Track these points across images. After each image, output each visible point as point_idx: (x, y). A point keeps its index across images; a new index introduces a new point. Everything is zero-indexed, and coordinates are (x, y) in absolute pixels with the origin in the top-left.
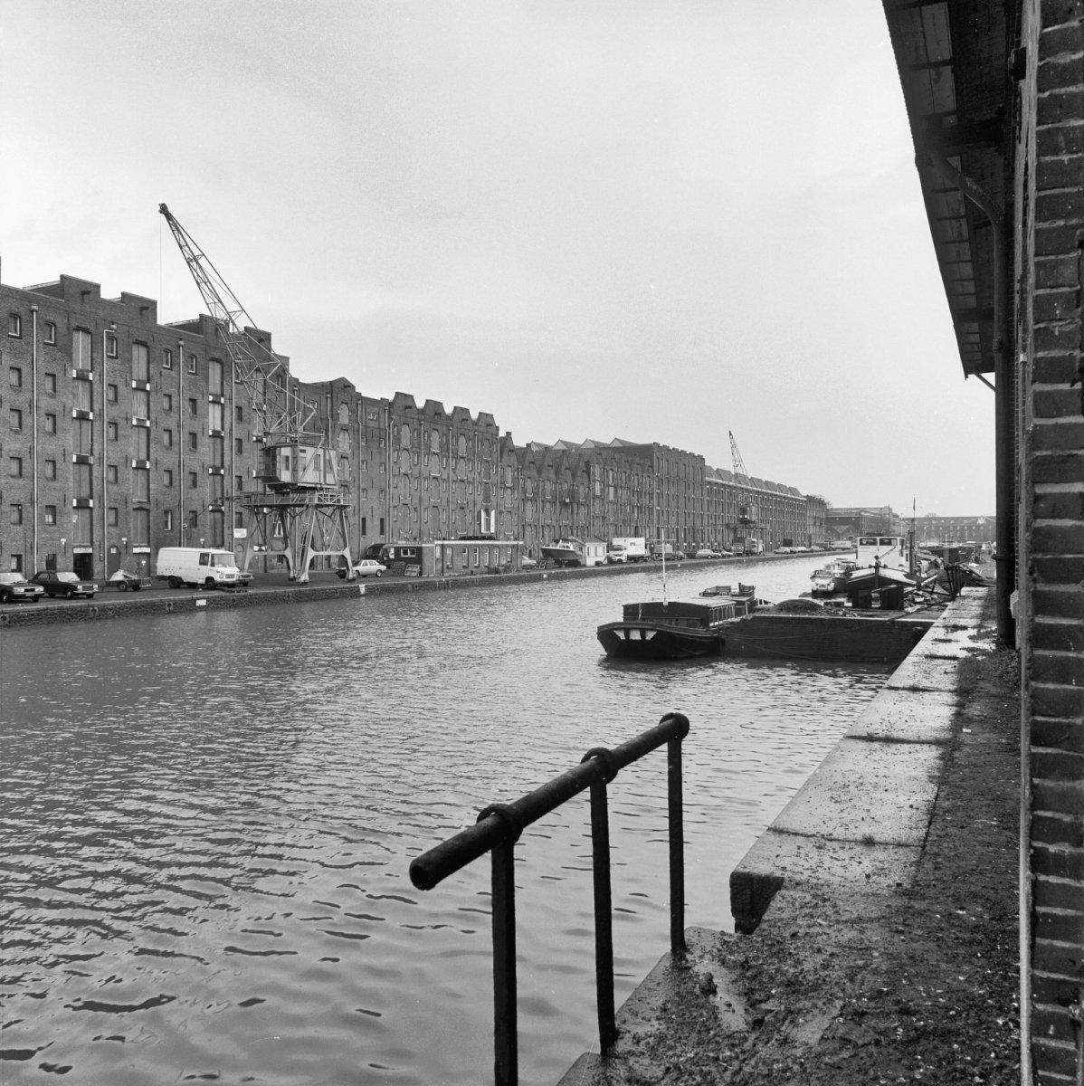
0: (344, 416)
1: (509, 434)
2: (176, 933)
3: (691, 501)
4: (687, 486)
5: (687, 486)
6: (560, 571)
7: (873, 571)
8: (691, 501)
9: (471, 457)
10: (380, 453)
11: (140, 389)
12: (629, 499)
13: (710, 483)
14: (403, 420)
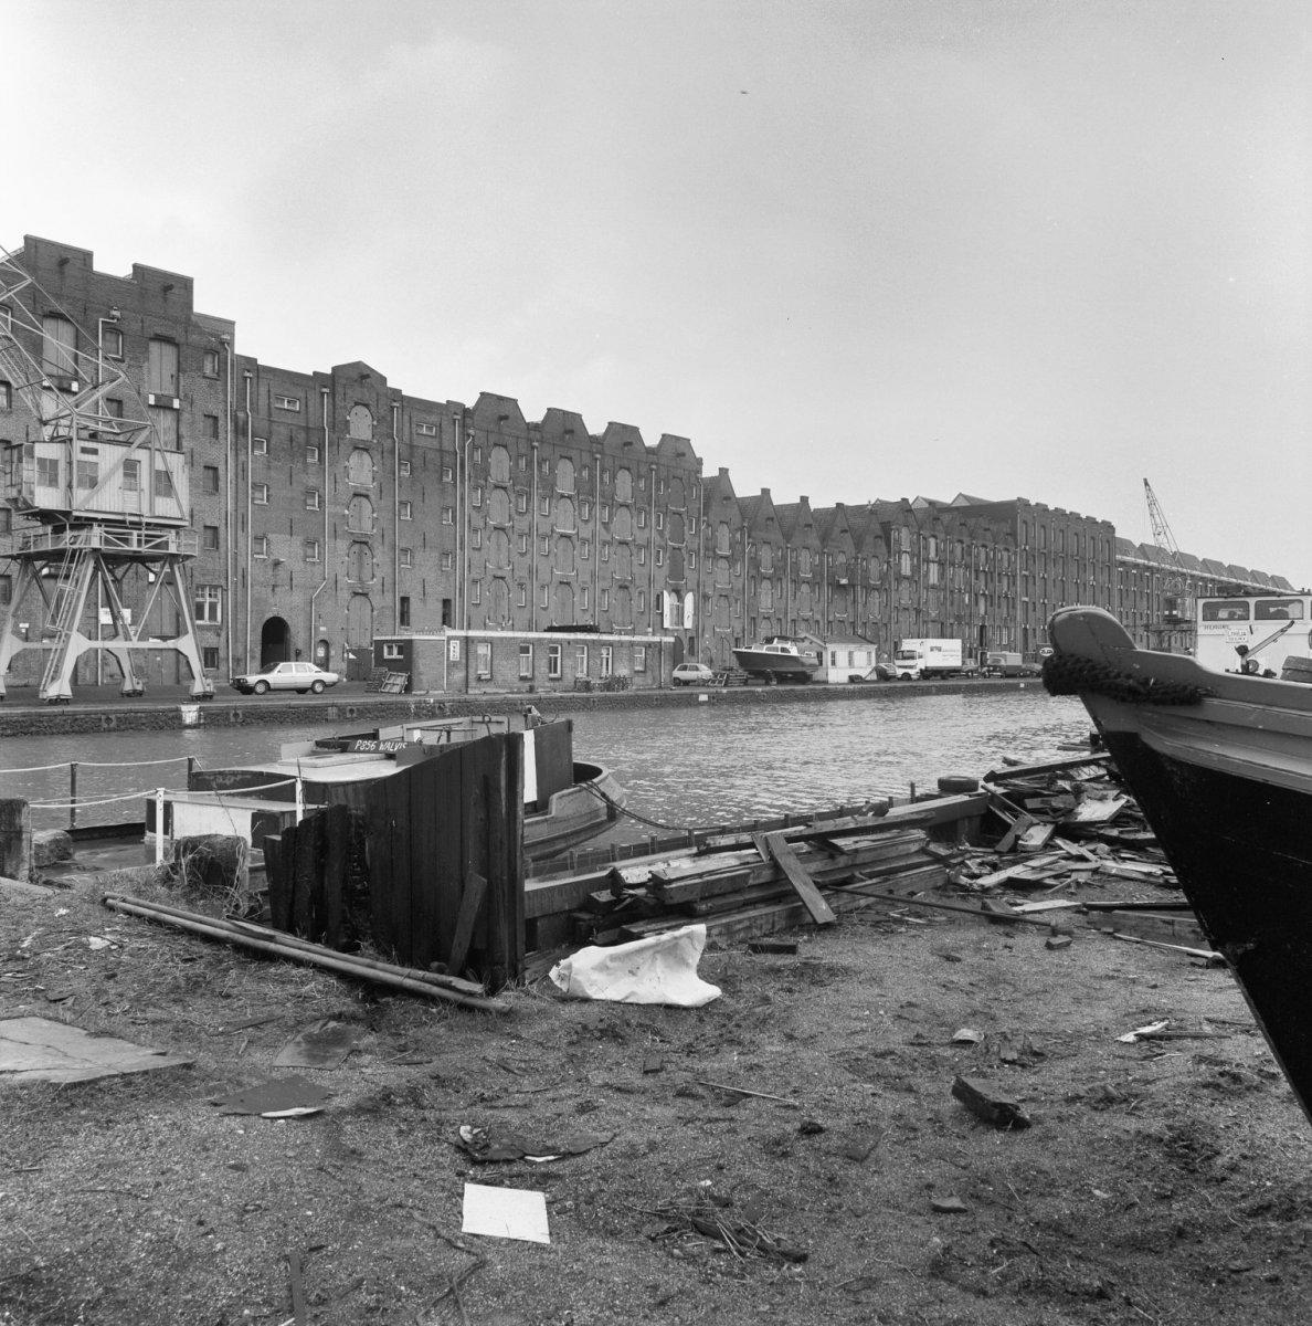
0: (361, 425)
1: (723, 471)
3: (1131, 596)
6: (768, 688)
8: (1131, 596)
10: (443, 491)
11: (162, 405)
13: (1123, 563)
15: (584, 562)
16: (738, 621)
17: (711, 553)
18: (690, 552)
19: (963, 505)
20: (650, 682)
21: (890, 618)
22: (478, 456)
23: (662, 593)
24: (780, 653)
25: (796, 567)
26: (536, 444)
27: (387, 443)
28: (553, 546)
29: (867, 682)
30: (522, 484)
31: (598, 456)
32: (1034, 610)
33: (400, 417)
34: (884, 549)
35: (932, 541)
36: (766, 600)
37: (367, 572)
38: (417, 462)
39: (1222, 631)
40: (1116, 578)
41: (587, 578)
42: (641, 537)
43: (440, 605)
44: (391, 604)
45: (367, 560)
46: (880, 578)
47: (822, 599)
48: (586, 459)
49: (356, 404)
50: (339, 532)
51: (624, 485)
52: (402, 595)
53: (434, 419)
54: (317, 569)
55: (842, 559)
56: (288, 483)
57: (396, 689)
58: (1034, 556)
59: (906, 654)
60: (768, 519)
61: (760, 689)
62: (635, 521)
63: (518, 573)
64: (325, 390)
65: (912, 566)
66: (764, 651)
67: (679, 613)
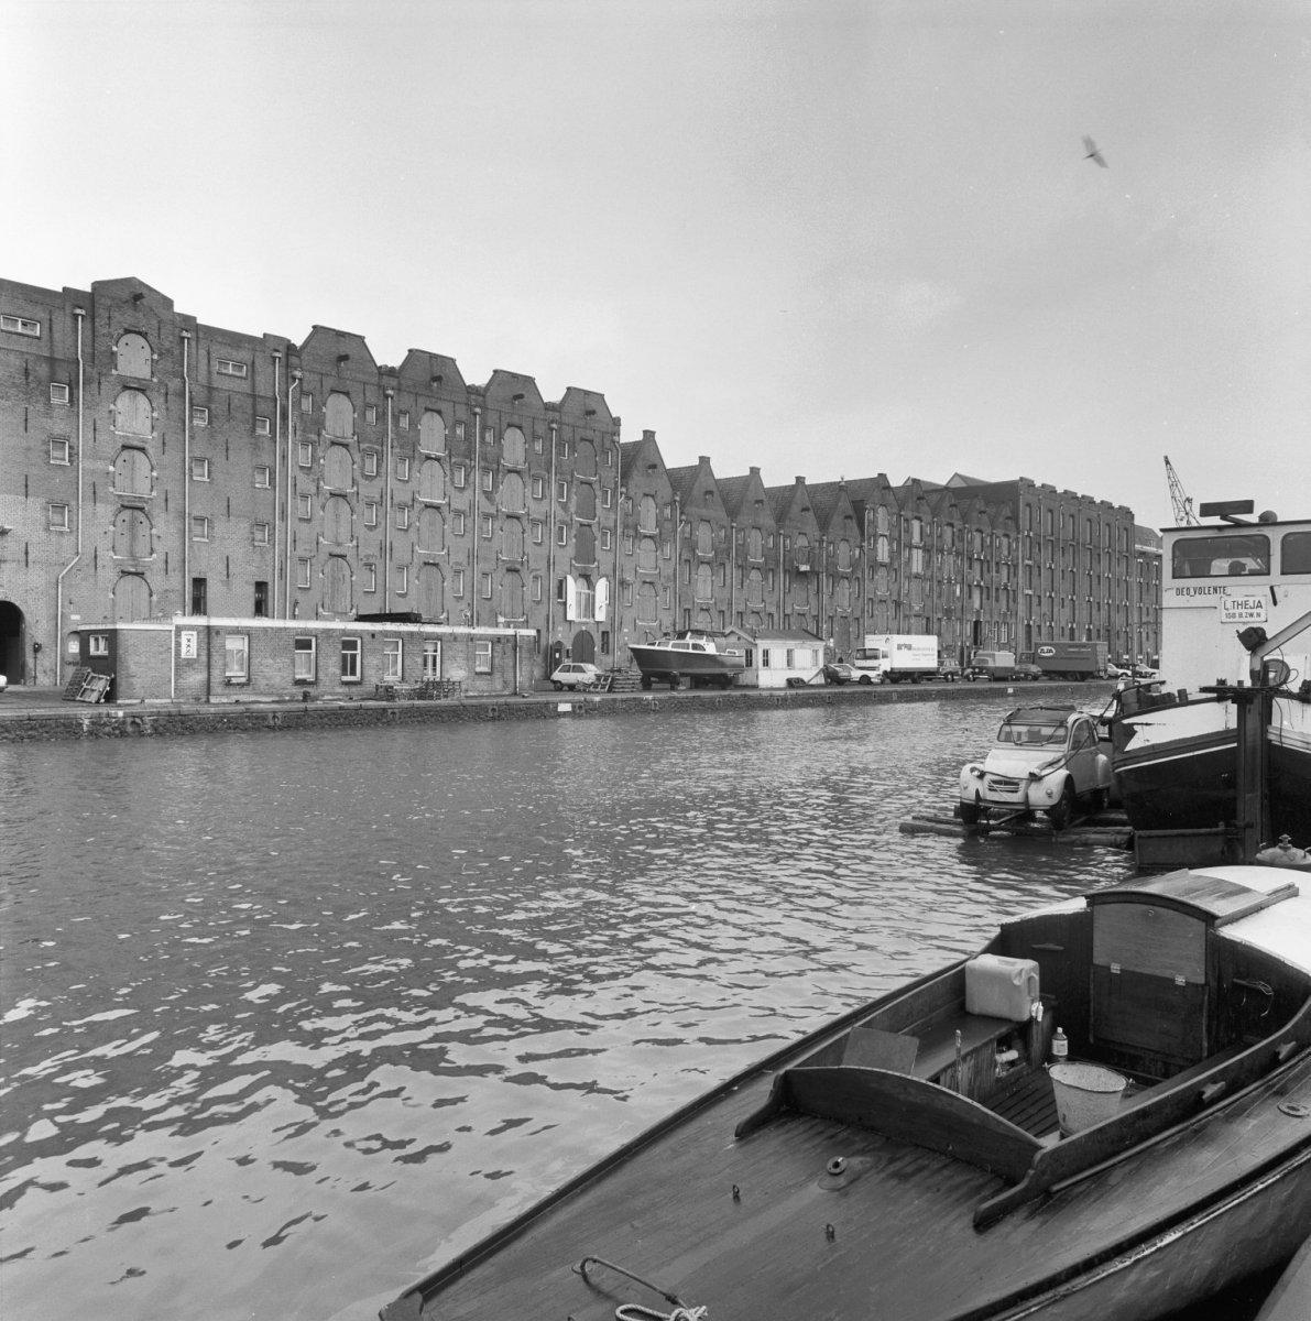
0: (134, 359)
1: (649, 435)
2: (454, 1102)
4: (1095, 555)
5: (1095, 555)
7: (1218, 718)
9: (533, 472)
12: (960, 572)
13: (1143, 554)
14: (329, 383)
15: (459, 539)
16: (667, 613)
17: (632, 532)
18: (603, 530)
19: (959, 486)
20: (499, 687)
21: (863, 612)
22: (307, 404)
23: (566, 578)
24: (691, 651)
25: (743, 550)
26: (390, 392)
27: (174, 384)
28: (414, 519)
29: (812, 686)
30: (370, 442)
31: (478, 410)
32: (1040, 604)
33: (194, 351)
34: (856, 530)
35: (916, 525)
36: (705, 586)
37: (142, 547)
38: (219, 407)
39: (1211, 599)
40: (1135, 570)
41: (462, 558)
42: (537, 510)
43: (252, 589)
44: (180, 587)
45: (143, 530)
46: (851, 565)
47: (776, 589)
48: (462, 413)
49: (127, 331)
50: (100, 493)
51: (514, 447)
52: (196, 575)
53: (244, 355)
54: (67, 541)
55: (802, 542)
56: (22, 429)
57: (93, 697)
58: (1039, 544)
59: (868, 653)
60: (757, 502)
61: (597, 699)
62: (528, 491)
63: (363, 552)
64: (78, 311)
65: (891, 552)
66: (669, 648)
67: (589, 606)
